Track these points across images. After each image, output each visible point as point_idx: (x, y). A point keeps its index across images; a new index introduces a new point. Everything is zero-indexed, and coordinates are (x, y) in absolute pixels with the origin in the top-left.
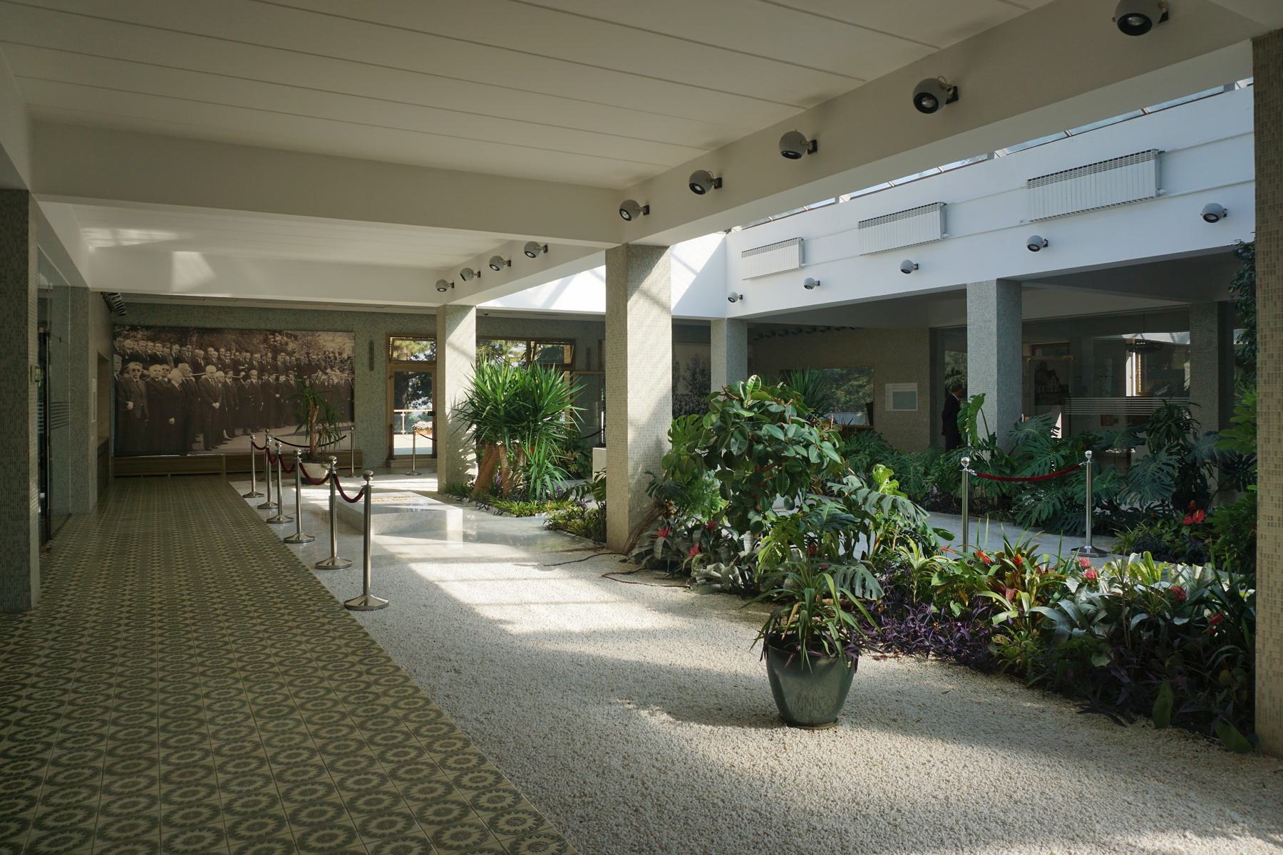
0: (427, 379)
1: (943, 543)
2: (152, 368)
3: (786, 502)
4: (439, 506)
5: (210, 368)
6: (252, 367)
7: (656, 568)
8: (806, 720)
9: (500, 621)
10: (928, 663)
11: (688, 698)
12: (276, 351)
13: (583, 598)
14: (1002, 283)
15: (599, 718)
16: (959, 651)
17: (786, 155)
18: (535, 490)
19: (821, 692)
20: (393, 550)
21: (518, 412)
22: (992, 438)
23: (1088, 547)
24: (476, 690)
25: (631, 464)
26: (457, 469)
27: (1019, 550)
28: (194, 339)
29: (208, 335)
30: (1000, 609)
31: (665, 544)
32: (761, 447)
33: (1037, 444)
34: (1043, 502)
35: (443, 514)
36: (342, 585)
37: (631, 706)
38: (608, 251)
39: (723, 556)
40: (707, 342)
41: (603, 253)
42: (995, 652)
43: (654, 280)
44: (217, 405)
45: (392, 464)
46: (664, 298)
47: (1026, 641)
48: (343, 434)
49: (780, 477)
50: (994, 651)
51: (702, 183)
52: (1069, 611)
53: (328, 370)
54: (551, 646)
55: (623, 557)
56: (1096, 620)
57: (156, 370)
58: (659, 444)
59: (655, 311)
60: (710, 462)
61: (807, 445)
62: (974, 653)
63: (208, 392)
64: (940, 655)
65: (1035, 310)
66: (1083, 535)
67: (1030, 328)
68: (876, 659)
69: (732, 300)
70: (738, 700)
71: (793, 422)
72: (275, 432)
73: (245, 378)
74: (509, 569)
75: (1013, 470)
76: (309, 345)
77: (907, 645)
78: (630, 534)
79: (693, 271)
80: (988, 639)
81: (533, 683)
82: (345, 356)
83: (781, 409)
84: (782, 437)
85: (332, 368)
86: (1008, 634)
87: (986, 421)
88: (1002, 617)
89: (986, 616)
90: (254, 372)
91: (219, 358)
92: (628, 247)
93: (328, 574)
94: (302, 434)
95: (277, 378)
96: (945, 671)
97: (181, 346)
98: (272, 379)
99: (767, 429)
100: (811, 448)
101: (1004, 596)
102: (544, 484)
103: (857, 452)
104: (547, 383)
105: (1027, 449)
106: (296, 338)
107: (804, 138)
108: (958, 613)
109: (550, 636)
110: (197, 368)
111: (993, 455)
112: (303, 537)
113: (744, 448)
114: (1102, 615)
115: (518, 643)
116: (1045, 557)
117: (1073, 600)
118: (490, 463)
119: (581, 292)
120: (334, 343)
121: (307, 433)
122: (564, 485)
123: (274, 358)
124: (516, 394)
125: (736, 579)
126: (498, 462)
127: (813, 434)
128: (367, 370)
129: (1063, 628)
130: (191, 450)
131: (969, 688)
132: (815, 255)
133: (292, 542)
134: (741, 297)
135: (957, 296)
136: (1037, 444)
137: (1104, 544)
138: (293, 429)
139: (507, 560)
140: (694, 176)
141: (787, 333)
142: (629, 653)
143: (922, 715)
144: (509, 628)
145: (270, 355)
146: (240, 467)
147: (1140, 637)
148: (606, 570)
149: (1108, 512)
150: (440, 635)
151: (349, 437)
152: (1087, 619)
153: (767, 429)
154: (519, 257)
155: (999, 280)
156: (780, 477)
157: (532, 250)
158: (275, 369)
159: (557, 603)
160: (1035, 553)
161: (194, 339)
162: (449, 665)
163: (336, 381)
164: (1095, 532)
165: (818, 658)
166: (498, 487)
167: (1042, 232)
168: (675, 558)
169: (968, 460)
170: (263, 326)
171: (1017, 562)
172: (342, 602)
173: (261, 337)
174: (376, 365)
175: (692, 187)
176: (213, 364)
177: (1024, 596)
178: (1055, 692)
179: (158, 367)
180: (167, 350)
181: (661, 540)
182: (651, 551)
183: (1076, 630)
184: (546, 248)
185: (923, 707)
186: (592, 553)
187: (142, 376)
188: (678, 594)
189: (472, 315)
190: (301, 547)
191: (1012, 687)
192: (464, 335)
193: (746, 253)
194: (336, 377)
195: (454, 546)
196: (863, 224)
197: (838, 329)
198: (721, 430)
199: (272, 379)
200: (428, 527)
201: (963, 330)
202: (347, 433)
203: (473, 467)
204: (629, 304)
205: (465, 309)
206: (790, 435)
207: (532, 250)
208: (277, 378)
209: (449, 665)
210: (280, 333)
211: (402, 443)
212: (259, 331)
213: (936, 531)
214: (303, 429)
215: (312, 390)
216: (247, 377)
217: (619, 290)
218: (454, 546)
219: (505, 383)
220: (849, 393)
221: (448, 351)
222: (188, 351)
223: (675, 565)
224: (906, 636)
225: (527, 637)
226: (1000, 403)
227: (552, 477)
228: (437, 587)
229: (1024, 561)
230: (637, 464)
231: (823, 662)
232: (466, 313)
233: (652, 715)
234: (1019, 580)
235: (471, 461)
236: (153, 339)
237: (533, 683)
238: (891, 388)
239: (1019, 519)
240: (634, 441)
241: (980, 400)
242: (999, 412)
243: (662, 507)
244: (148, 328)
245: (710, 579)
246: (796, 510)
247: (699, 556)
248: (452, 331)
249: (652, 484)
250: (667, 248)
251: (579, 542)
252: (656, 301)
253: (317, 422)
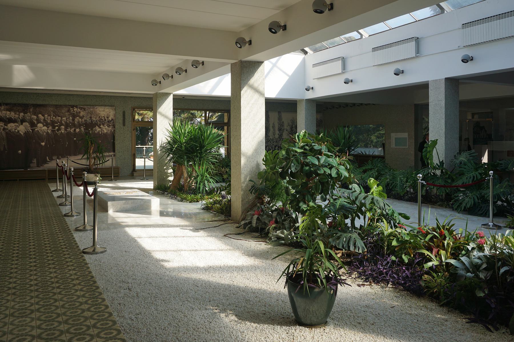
0: (145, 132)
1: (403, 220)
2: (9, 125)
3: (322, 197)
4: (146, 196)
5: (40, 125)
6: (62, 124)
7: (254, 232)
8: (308, 322)
9: (163, 261)
10: (387, 289)
11: (249, 306)
12: (74, 116)
13: (211, 248)
14: (448, 80)
15: (197, 318)
16: (405, 283)
17: (316, 11)
18: (199, 188)
19: (315, 308)
20: (119, 220)
21: (192, 148)
22: (442, 163)
23: (491, 224)
24: (136, 301)
25: (243, 176)
26: (163, 176)
27: (444, 227)
28: (31, 110)
29: (38, 108)
30: (430, 260)
31: (258, 219)
32: (307, 168)
33: (466, 167)
34: (466, 198)
35: (149, 201)
36: (83, 240)
37: (216, 311)
38: (232, 64)
39: (287, 226)
40: (295, 111)
41: (230, 65)
42: (423, 285)
43: (256, 79)
44: (43, 144)
45: (135, 174)
46: (261, 89)
47: (440, 279)
48: (107, 159)
49: (308, 187)
50: (423, 284)
51: (275, 28)
52: (466, 263)
53: (102, 126)
54: (184, 275)
55: (237, 225)
56: (481, 269)
57: (11, 126)
58: (258, 165)
59: (256, 96)
60: (283, 176)
61: (331, 167)
62: (412, 283)
63: (39, 137)
64: (395, 285)
65: (467, 94)
66: (489, 217)
67: (464, 105)
68: (359, 286)
69: (307, 90)
70: (276, 309)
71: (325, 155)
72: (73, 158)
73: (58, 130)
74: (177, 231)
75: (453, 180)
76: (91, 113)
77: (376, 278)
78: (242, 213)
79: (288, 75)
80: (421, 276)
81: (168, 297)
82: (110, 119)
83: (320, 147)
84: (317, 163)
85: (103, 125)
86: (431, 275)
87: (439, 154)
88: (430, 264)
89: (420, 264)
90: (63, 127)
91: (44, 120)
92: (241, 62)
93: (81, 234)
94: (85, 159)
95: (75, 130)
96: (396, 294)
97: (24, 113)
98: (72, 130)
99: (312, 159)
100: (333, 169)
101: (432, 253)
102: (204, 186)
103: (371, 169)
104: (207, 133)
105: (461, 169)
106: (84, 109)
107: (326, 3)
108: (406, 261)
109: (186, 269)
110: (33, 125)
111: (442, 172)
112: (74, 213)
113: (298, 169)
114: (484, 266)
115: (168, 273)
116: (460, 230)
117: (468, 257)
118: (179, 174)
119: (219, 86)
120: (105, 112)
121: (88, 158)
122: (213, 185)
123: (73, 120)
124: (191, 139)
125: (292, 238)
126: (182, 174)
127: (334, 161)
128: (122, 126)
129: (462, 272)
130: (30, 167)
131: (407, 305)
132: (350, 66)
133: (68, 216)
134: (312, 88)
135: (424, 87)
136: (466, 167)
137: (500, 221)
138: (80, 157)
139: (177, 226)
140: (271, 24)
141: (340, 106)
142: (225, 279)
143: (376, 320)
144: (166, 264)
145: (71, 118)
146: (53, 176)
147: (506, 279)
148: (228, 232)
149: (505, 204)
150: (128, 268)
151: (111, 160)
152: (476, 268)
153: (312, 159)
154: (191, 69)
155: (446, 79)
156: (308, 187)
157: (195, 64)
158: (74, 125)
159: (196, 250)
160: (453, 228)
161: (31, 110)
162: (126, 286)
163: (105, 131)
164: (494, 215)
165: (314, 288)
166: (183, 186)
167: (469, 52)
168: (264, 226)
169: (421, 176)
170: (67, 104)
171: (441, 234)
172: (82, 249)
173: (67, 109)
174: (127, 123)
175: (270, 30)
176: (41, 123)
177: (443, 252)
178: (456, 309)
179: (12, 124)
180: (17, 116)
181: (256, 217)
182: (250, 223)
183: (469, 274)
184: (203, 63)
185: (378, 316)
186: (223, 223)
187: (4, 129)
188: (261, 246)
189: (171, 98)
190: (73, 218)
191: (432, 305)
192: (167, 108)
193: (315, 65)
194: (106, 129)
195: (155, 218)
196: (375, 49)
197: (366, 105)
198: (287, 159)
199: (72, 130)
200: (140, 208)
201: (427, 105)
202: (110, 158)
203: (171, 176)
204: (242, 92)
205: (167, 95)
206: (322, 162)
207: (195, 64)
208: (75, 130)
209: (126, 286)
210: (76, 107)
211: (139, 163)
212: (66, 106)
213: (400, 214)
214: (85, 157)
215: (92, 137)
216: (59, 129)
217: (237, 86)
218: (155, 218)
219: (185, 133)
220: (378, 137)
221: (158, 116)
222: (28, 116)
223: (263, 229)
224: (376, 273)
225: (174, 269)
226: (446, 144)
227: (208, 181)
228: (135, 241)
229: (446, 233)
230: (246, 176)
231: (317, 290)
232: (168, 97)
233: (226, 316)
234: (441, 244)
235: (170, 173)
236: (10, 110)
237: (168, 297)
238: (393, 135)
239: (455, 207)
240: (245, 164)
241: (435, 142)
242: (446, 149)
243: (259, 199)
244: (7, 104)
245: (279, 238)
246: (327, 202)
247: (274, 226)
248: (160, 107)
249: (252, 187)
250: (262, 62)
251: (218, 216)
252: (256, 90)
253: (93, 153)
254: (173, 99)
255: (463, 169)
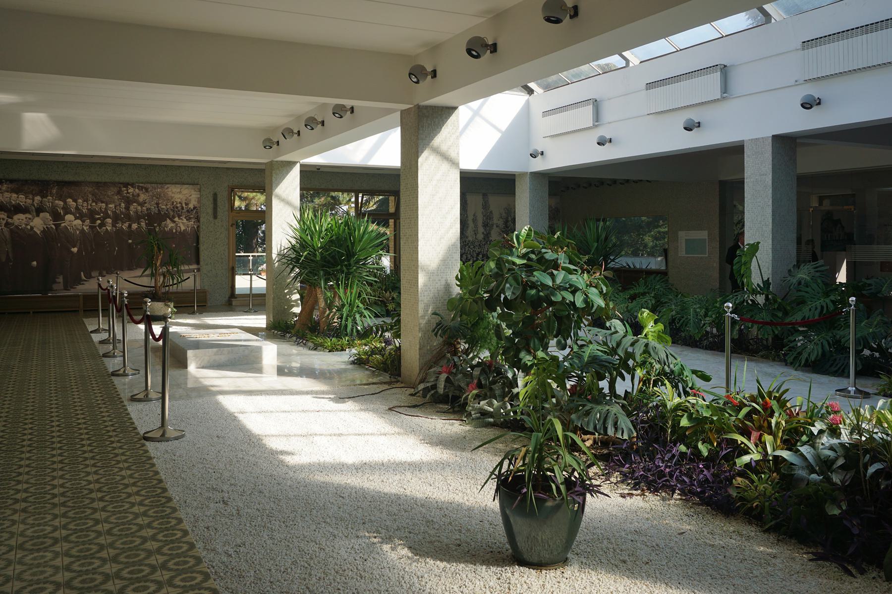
0: (252, 230)
1: (699, 383)
2: (16, 217)
3: (559, 343)
4: (254, 341)
5: (69, 217)
6: (107, 216)
7: (441, 402)
8: (535, 559)
9: (282, 453)
10: (672, 502)
11: (432, 532)
12: (129, 202)
13: (365, 431)
14: (778, 139)
15: (343, 552)
16: (703, 492)
17: (548, 20)
18: (346, 326)
19: (547, 534)
20: (207, 382)
21: (333, 257)
22: (767, 283)
23: (852, 389)
24: (236, 523)
25: (421, 306)
26: (282, 306)
27: (770, 394)
28: (54, 191)
29: (67, 187)
30: (746, 452)
31: (448, 380)
32: (533, 292)
33: (808, 289)
34: (809, 344)
35: (259, 350)
36: (144, 417)
37: (376, 540)
38: (402, 112)
39: (498, 392)
40: (512, 193)
41: (399, 113)
42: (735, 494)
43: (444, 137)
44: (75, 250)
45: (234, 303)
46: (452, 154)
47: (763, 485)
48: (186, 276)
49: (535, 324)
50: (734, 493)
51: (477, 48)
52: (808, 456)
53: (176, 219)
54: (320, 478)
55: (412, 391)
56: (835, 466)
57: (19, 219)
58: (447, 287)
59: (445, 166)
60: (491, 305)
61: (574, 290)
62: (715, 492)
63: (67, 238)
64: (686, 495)
65: (811, 163)
66: (848, 377)
67: (806, 183)
68: (623, 496)
69: (533, 156)
70: (479, 537)
71: (564, 269)
72: (126, 274)
73: (101, 226)
74: (308, 401)
75: (786, 313)
76: (158, 196)
77: (653, 483)
78: (421, 370)
79: (499, 130)
80: (730, 480)
81: (292, 515)
82: (191, 206)
83: (555, 256)
84: (550, 284)
85: (179, 216)
86: (748, 478)
87: (761, 268)
88: (746, 459)
89: (730, 458)
90: (109, 221)
91: (77, 208)
92: (419, 107)
93: (140, 406)
94: (147, 276)
95: (130, 226)
96: (687, 511)
97: (42, 197)
98: (125, 226)
99: (541, 277)
100: (578, 294)
101: (749, 439)
102: (355, 322)
103: (644, 294)
104: (359, 231)
105: (800, 294)
106: (147, 190)
107: (566, 5)
108: (705, 453)
109: (322, 467)
110: (57, 217)
111: (767, 299)
112: (129, 371)
113: (518, 293)
114: (841, 462)
115: (291, 474)
116: (799, 400)
117: (813, 446)
118: (310, 303)
119: (380, 149)
120: (182, 194)
121: (152, 275)
122: (370, 321)
123: (127, 208)
124: (331, 241)
125: (507, 414)
126: (316, 302)
127: (580, 280)
128: (211, 219)
129: (802, 473)
130: (51, 290)
131: (706, 529)
132: (608, 114)
133: (118, 375)
134: (542, 153)
135: (735, 151)
136: (808, 289)
137: (868, 385)
138: (139, 272)
139: (307, 393)
140: (470, 42)
141: (590, 185)
142: (390, 485)
143: (653, 557)
144: (288, 459)
145: (123, 205)
146: (91, 306)
147: (878, 485)
148: (395, 403)
149: (877, 355)
150: (221, 466)
151: (192, 278)
152: (826, 465)
153: (541, 277)
154: (331, 120)
155: (775, 137)
156: (535, 324)
157: (339, 111)
158: (128, 218)
159: (340, 435)
160: (786, 396)
161: (54, 191)
162: (218, 496)
163: (183, 228)
164: (858, 374)
165: (545, 501)
166: (318, 323)
167: (814, 91)
168: (457, 393)
169: (731, 305)
170: (117, 180)
171: (765, 407)
172: (142, 433)
173: (115, 190)
174: (220, 214)
175: (469, 51)
176: (71, 213)
177: (768, 438)
178: (791, 537)
179: (21, 216)
180: (29, 201)
181: (443, 376)
182: (434, 387)
183: (814, 476)
184: (352, 110)
185: (656, 548)
186: (386, 387)
187: (7, 224)
188: (454, 427)
189: (296, 170)
190: (127, 379)
191: (749, 530)
192: (289, 187)
193: (546, 113)
194: (183, 225)
195: (270, 379)
196: (650, 86)
197: (636, 182)
198: (498, 275)
199: (125, 226)
200: (244, 360)
201: (741, 183)
202: (191, 275)
203: (298, 306)
204: (420, 160)
205: (290, 164)
206: (559, 281)
207: (339, 111)
208: (130, 226)
209: (218, 496)
210: (133, 185)
211: (242, 282)
212: (114, 184)
213: (694, 372)
214: (148, 272)
215: (160, 238)
216: (103, 225)
217: (412, 149)
218: (270, 379)
219: (321, 231)
220: (656, 238)
221: (275, 202)
222: (48, 201)
223: (456, 398)
224: (653, 475)
225: (302, 468)
226: (774, 250)
227: (362, 315)
228: (235, 419)
229: (774, 404)
230: (427, 306)
231: (550, 504)
232: (291, 169)
233: (393, 549)
234: (766, 424)
235: (296, 301)
236: (17, 191)
237: (292, 515)
238: (683, 235)
239: (790, 360)
240: (425, 285)
241: (755, 247)
242: (774, 259)
243: (450, 345)
244: (12, 181)
245: (484, 414)
246: (568, 350)
247: (475, 392)
248: (277, 186)
249: (438, 324)
250: (455, 108)
251: (378, 376)
252: (445, 157)
253: (162, 265)
254: (301, 171)
255: (803, 294)
